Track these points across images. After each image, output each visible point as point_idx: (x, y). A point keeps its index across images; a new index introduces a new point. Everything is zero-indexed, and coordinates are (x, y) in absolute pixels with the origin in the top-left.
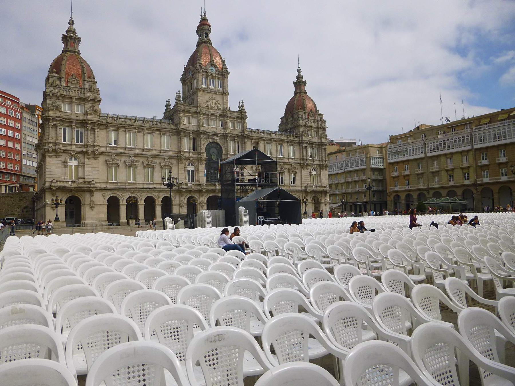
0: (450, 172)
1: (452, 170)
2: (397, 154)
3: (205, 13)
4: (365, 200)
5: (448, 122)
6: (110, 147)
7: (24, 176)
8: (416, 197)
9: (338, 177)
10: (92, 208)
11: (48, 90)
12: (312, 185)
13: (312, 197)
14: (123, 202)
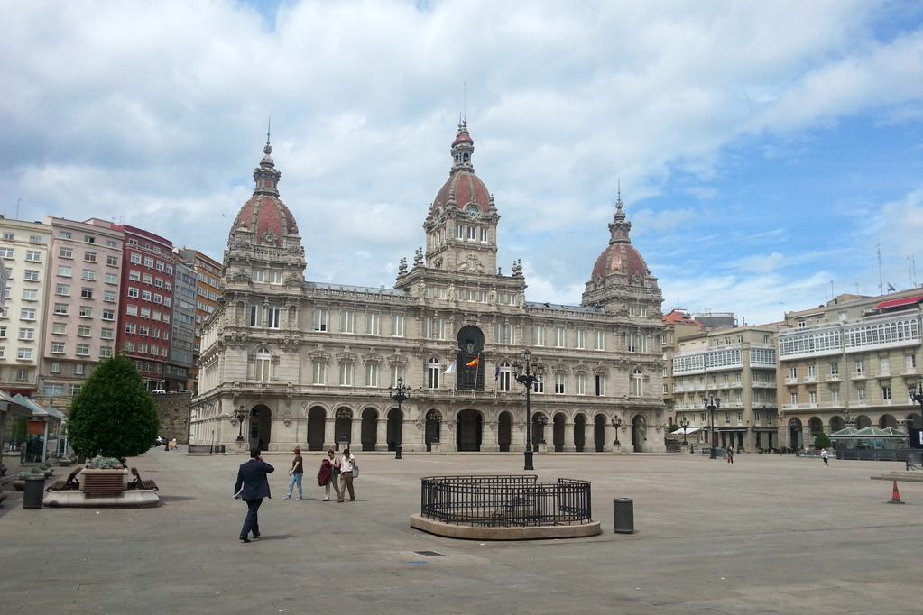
0: (885, 385)
1: (888, 379)
2: (795, 347)
3: (465, 122)
4: (740, 425)
5: (893, 292)
6: (316, 334)
7: (172, 365)
8: (828, 424)
9: (842, 364)
10: (288, 424)
11: (234, 253)
12: (632, 396)
13: (633, 416)
14: (330, 415)
